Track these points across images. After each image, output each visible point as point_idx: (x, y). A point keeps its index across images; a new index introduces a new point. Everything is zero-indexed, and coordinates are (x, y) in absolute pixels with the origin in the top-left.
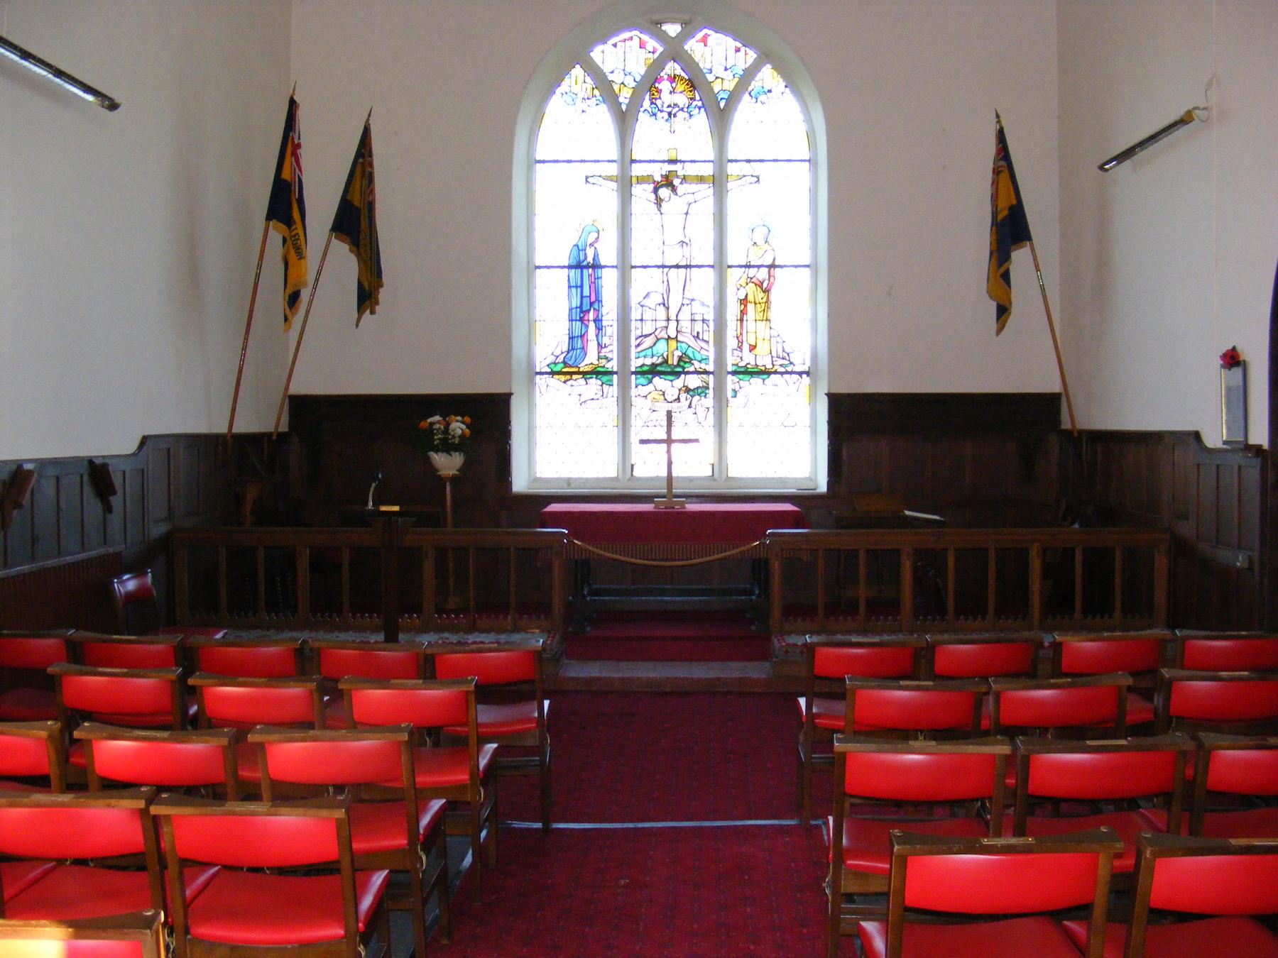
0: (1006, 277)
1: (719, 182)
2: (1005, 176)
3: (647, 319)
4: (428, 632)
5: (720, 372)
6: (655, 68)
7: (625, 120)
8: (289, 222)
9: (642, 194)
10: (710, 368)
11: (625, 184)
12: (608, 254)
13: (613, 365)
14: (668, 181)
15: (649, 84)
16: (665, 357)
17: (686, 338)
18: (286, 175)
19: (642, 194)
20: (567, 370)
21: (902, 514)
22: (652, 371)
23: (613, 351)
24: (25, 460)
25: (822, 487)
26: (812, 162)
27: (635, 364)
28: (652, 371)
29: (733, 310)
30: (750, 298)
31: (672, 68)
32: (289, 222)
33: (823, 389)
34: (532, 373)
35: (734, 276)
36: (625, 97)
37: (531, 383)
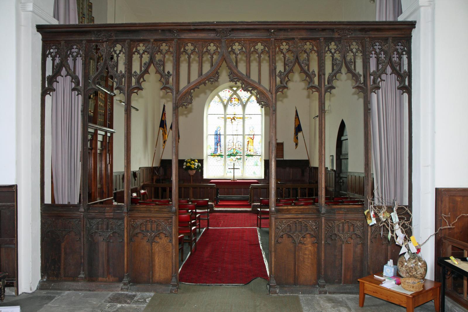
0: (297, 138)
1: (244, 119)
2: (297, 119)
3: (229, 145)
6: (232, 95)
7: (225, 107)
8: (164, 128)
9: (229, 121)
12: (222, 132)
13: (223, 154)
14: (234, 119)
15: (230, 99)
19: (229, 121)
20: (214, 155)
25: (263, 178)
27: (227, 154)
28: (231, 155)
29: (246, 143)
30: (380, 47)
31: (235, 96)
32: (164, 128)
33: (263, 159)
35: (246, 137)
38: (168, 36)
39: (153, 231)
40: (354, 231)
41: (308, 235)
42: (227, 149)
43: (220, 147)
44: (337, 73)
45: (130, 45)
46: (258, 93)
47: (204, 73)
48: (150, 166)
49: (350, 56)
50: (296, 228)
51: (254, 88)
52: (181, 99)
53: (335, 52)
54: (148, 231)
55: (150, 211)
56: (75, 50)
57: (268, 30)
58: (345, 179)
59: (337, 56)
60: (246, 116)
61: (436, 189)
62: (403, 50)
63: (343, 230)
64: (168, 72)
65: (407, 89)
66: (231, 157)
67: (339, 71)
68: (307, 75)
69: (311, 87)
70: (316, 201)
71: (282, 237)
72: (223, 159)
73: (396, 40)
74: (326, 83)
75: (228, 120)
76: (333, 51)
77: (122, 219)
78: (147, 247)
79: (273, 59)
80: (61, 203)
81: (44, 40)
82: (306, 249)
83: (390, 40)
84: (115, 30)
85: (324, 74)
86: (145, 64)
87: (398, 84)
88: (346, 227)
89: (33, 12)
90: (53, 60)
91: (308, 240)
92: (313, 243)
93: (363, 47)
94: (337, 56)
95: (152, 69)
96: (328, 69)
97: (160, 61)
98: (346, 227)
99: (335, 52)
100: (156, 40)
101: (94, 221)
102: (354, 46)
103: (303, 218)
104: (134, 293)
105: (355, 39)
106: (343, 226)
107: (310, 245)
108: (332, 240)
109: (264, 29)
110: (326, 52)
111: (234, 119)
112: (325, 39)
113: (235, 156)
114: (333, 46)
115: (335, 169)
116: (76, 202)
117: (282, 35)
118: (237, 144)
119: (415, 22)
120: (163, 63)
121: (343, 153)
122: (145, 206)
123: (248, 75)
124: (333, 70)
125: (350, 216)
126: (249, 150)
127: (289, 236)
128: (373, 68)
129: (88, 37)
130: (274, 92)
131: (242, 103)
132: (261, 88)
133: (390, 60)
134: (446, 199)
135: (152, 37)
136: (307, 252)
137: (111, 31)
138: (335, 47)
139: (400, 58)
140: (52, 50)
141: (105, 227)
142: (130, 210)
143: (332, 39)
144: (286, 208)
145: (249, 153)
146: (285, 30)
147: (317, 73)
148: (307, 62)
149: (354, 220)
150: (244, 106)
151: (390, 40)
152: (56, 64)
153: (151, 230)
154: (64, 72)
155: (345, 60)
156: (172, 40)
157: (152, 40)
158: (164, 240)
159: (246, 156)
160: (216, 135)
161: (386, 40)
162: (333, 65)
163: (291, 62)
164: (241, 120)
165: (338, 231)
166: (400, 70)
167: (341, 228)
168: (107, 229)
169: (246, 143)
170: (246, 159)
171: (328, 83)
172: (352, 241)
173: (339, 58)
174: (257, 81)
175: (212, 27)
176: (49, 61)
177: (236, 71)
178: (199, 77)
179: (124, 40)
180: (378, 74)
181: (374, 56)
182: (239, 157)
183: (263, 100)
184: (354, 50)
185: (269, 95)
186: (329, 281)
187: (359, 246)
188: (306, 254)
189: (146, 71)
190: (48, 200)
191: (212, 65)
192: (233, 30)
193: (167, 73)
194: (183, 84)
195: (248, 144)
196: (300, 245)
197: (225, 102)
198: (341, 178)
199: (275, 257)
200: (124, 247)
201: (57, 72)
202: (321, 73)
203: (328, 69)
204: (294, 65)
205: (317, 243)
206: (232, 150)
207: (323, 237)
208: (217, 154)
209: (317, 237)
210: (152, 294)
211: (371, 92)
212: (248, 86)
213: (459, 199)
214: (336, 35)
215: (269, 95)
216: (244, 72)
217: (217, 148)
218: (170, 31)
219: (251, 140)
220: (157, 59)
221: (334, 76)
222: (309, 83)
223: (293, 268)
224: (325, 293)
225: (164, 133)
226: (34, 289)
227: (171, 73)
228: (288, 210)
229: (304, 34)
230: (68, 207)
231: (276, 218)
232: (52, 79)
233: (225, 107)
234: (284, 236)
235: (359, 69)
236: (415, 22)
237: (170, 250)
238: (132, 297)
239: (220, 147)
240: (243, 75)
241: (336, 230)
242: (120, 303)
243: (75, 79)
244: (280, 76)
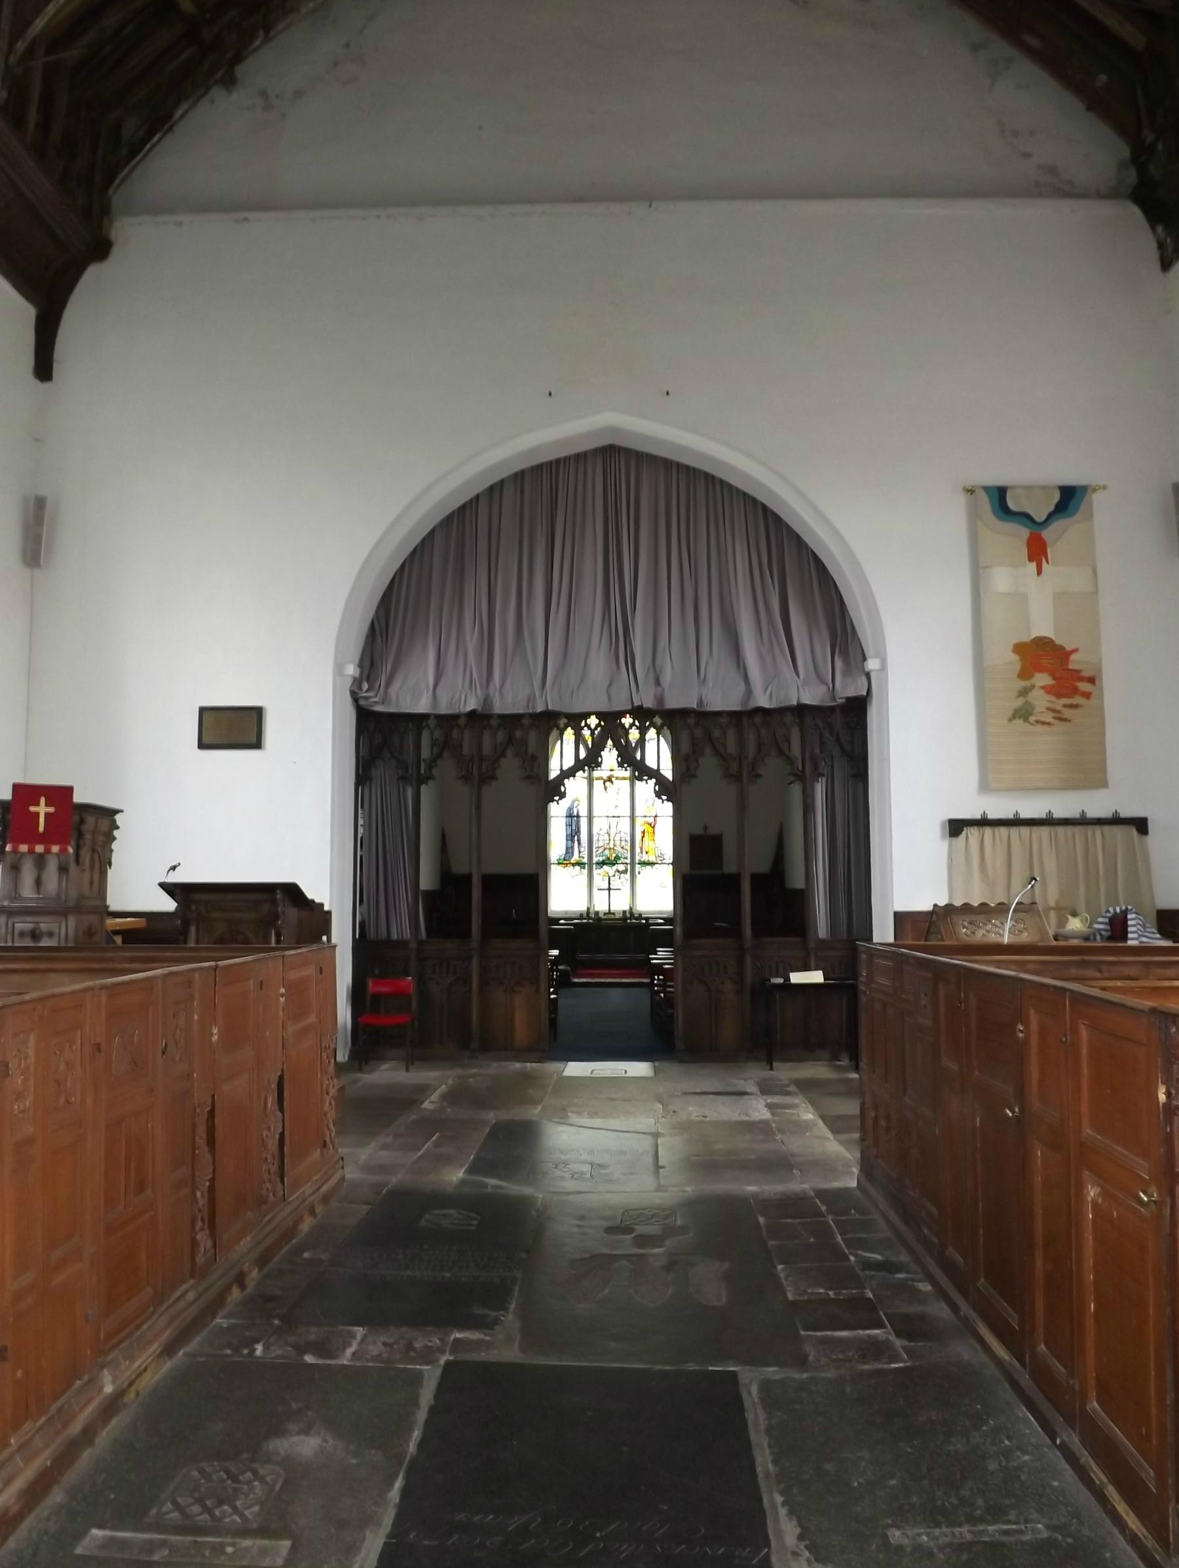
3: (600, 840)
14: (610, 779)
17: (618, 848)
23: (585, 854)
27: (595, 860)
28: (602, 864)
42: (594, 850)
43: (579, 843)
66: (605, 866)
68: (724, 759)
72: (585, 871)
113: (614, 864)
118: (617, 838)
126: (644, 852)
145: (645, 858)
159: (639, 864)
170: (639, 873)
182: (621, 867)
195: (643, 837)
206: (607, 852)
208: (573, 861)
217: (572, 847)
219: (650, 829)
239: (579, 843)
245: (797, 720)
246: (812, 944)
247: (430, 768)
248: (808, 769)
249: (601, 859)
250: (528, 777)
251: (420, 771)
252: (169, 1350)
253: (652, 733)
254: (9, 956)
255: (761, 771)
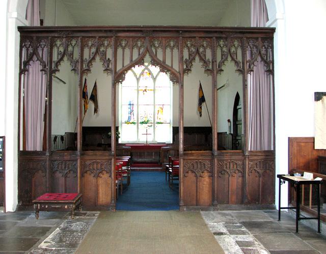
0: (201, 108)
1: (154, 90)
2: (201, 91)
3: (141, 114)
4: (46, 233)
5: (154, 123)
6: (143, 71)
7: (138, 79)
8: (85, 99)
9: (141, 92)
10: (153, 122)
11: (138, 91)
12: (135, 103)
13: (136, 122)
14: (145, 90)
15: (142, 73)
16: (309, 233)
17: (149, 117)
18: (85, 91)
19: (141, 92)
20: (127, 123)
21: (271, 205)
22: (143, 123)
23: (136, 119)
24: (322, 93)
25: (172, 142)
26: (170, 87)
27: (139, 122)
28: (143, 123)
29: (156, 112)
30: (253, 43)
31: (146, 71)
32: (85, 99)
33: (172, 126)
34: (122, 123)
35: (156, 107)
36: (138, 77)
37: (122, 125)
38: (109, 34)
39: (98, 169)
40: (237, 168)
41: (206, 171)
44: (225, 60)
45: (82, 40)
46: (171, 74)
47: (133, 60)
48: (73, 132)
49: (233, 49)
50: (197, 166)
51: (168, 70)
52: (117, 77)
53: (223, 47)
54: (94, 169)
55: (96, 155)
56: (43, 43)
57: (178, 31)
58: (240, 141)
59: (225, 49)
60: (156, 88)
61: (289, 138)
62: (268, 46)
63: (229, 168)
64: (109, 59)
65: (271, 72)
67: (226, 59)
68: (205, 62)
69: (207, 71)
70: (211, 149)
71: (187, 172)
73: (263, 39)
74: (218, 67)
75: (140, 92)
76: (222, 46)
77: (76, 160)
78: (94, 181)
79: (181, 51)
80: (30, 150)
81: (21, 37)
82: (204, 180)
83: (260, 39)
84: (71, 31)
85: (216, 61)
86: (93, 53)
87: (265, 68)
88: (231, 165)
89: (17, 18)
90: (27, 50)
91: (206, 175)
92: (209, 177)
93: (242, 43)
94: (225, 49)
95: (98, 58)
96: (219, 59)
97: (103, 51)
98: (231, 165)
99: (223, 47)
100: (100, 37)
101: (56, 163)
102: (236, 43)
103: (203, 159)
104: (85, 212)
105: (236, 38)
106: (230, 165)
107: (207, 178)
108: (222, 174)
109: (175, 31)
110: (217, 47)
111: (145, 90)
112: (217, 38)
114: (222, 43)
115: (232, 133)
116: (39, 148)
117: (187, 35)
119: (275, 28)
120: (105, 54)
121: (238, 119)
122: (92, 152)
123: (164, 62)
124: (222, 58)
125: (234, 157)
127: (193, 172)
128: (248, 58)
129: (53, 35)
130: (182, 73)
131: (153, 77)
132: (173, 71)
133: (260, 52)
134: (295, 144)
135: (98, 35)
136: (205, 183)
137: (68, 31)
138: (223, 43)
139: (267, 51)
140: (26, 43)
141: (63, 167)
142: (82, 154)
143: (220, 38)
144: (190, 152)
145: (159, 121)
146: (190, 32)
147: (211, 60)
148: (204, 53)
149: (237, 160)
150: (155, 79)
151: (260, 39)
152: (29, 53)
153: (97, 168)
154: (35, 58)
155: (230, 52)
156: (112, 37)
157: (97, 37)
158: (105, 176)
160: (130, 105)
161: (257, 39)
162: (222, 55)
163: (193, 53)
164: (153, 92)
165: (226, 168)
166: (267, 59)
167: (228, 166)
168: (65, 168)
169: (156, 112)
171: (219, 68)
172: (235, 175)
173: (226, 51)
174: (170, 65)
175: (140, 29)
176: (24, 50)
177: (156, 59)
178: (130, 62)
179: (78, 37)
180: (252, 63)
181: (249, 49)
183: (176, 79)
184: (236, 45)
185: (178, 75)
186: (221, 202)
187: (240, 179)
188: (204, 184)
189: (94, 58)
190: (21, 149)
191: (139, 54)
192: (154, 31)
193: (107, 59)
194: (119, 67)
196: (200, 178)
197: (138, 77)
198: (237, 140)
199: (183, 186)
200: (77, 180)
201: (30, 58)
202: (214, 61)
203: (219, 59)
204: (196, 55)
205: (212, 176)
207: (216, 172)
208: (131, 122)
209: (211, 172)
210: (99, 212)
211: (248, 73)
212: (164, 68)
213: (303, 144)
214: (224, 36)
215: (178, 75)
216: (161, 59)
218: (110, 31)
220: (101, 50)
221: (222, 62)
222: (206, 67)
223: (195, 194)
224: (218, 210)
225: (86, 103)
226: (15, 210)
227: (111, 59)
228: (192, 154)
229: (203, 35)
230: (35, 153)
231: (184, 160)
232: (26, 63)
233: (138, 79)
234: (189, 172)
235: (240, 58)
236: (275, 28)
237: (110, 182)
238: (85, 214)
240: (160, 61)
241: (225, 167)
242: (78, 216)
243: (42, 62)
244: (186, 62)
245: (240, 44)
246: (247, 154)
247: (57, 65)
248: (246, 67)
249: (142, 121)
250: (106, 70)
251: (51, 67)
252: (47, 246)
253: (168, 50)
254: (139, 167)
255: (223, 68)
